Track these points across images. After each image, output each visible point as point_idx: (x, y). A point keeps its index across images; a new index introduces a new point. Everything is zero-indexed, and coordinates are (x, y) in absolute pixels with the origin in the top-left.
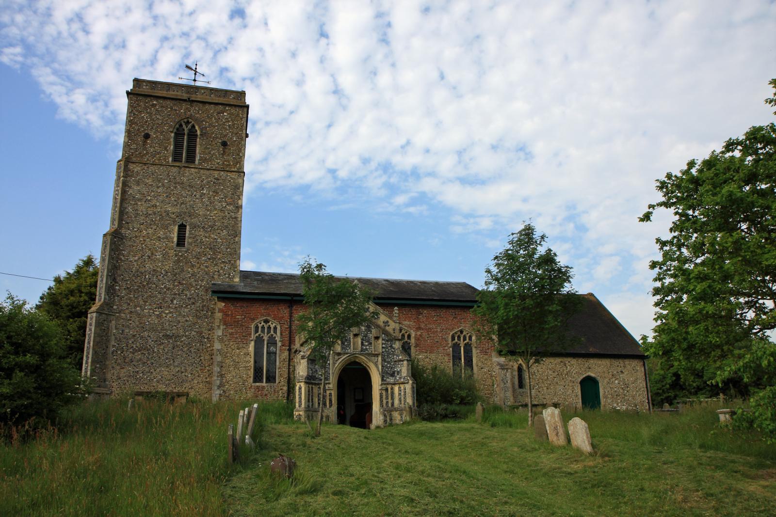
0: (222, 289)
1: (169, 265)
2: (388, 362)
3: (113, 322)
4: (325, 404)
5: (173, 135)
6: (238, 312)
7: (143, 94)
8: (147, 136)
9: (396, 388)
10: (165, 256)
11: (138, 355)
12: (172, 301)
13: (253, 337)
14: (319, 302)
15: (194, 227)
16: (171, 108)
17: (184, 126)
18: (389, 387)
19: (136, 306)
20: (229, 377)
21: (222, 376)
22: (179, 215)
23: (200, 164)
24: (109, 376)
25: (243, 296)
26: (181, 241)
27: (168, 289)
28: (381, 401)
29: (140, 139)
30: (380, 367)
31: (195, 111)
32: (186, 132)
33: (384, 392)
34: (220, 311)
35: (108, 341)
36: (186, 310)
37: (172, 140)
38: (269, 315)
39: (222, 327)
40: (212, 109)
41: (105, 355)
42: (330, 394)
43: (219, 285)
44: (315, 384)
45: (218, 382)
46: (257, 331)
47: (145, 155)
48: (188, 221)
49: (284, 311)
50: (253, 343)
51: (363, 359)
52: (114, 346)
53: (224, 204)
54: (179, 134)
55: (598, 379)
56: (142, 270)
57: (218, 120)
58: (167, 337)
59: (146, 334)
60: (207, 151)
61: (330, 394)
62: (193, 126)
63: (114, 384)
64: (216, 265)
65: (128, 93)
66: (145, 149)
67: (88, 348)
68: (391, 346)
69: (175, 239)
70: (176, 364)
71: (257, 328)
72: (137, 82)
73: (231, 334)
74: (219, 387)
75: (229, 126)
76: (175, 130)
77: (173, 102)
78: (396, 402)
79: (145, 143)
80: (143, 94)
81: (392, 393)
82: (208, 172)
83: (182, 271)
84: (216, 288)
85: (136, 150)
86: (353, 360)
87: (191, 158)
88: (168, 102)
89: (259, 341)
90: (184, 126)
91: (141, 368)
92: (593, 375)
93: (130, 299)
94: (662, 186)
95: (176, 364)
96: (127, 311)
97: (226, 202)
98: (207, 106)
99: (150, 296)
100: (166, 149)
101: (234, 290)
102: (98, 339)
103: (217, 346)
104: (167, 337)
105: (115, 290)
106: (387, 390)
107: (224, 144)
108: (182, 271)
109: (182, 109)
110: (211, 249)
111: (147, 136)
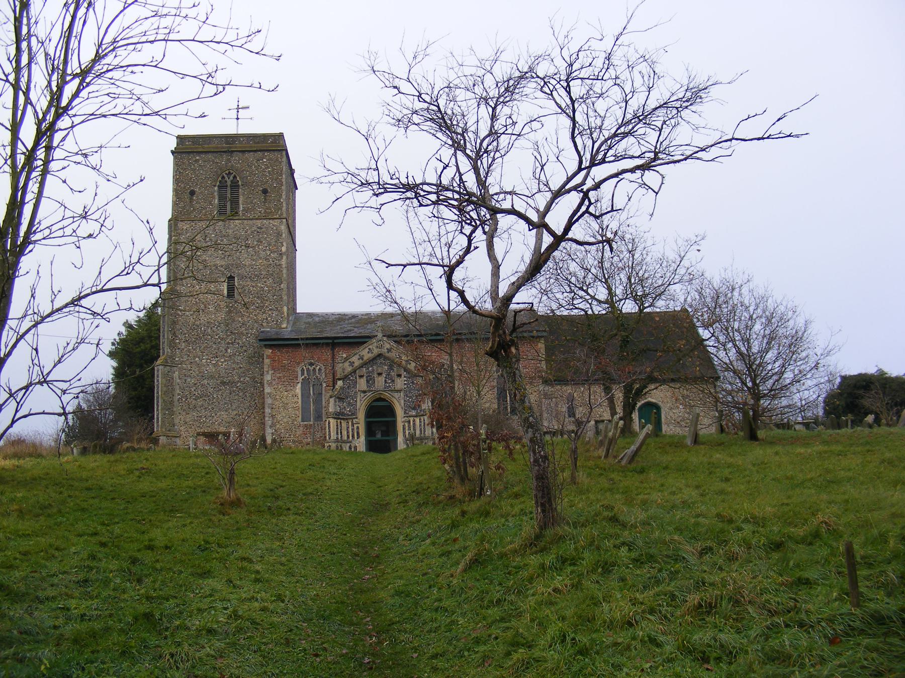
0: (269, 336)
1: (221, 316)
2: (410, 397)
3: (177, 373)
4: (353, 436)
5: (216, 188)
6: (285, 357)
7: (189, 150)
8: (192, 193)
9: (417, 420)
10: (218, 308)
11: (200, 402)
12: (226, 350)
13: (300, 379)
14: (337, 338)
15: (242, 277)
16: (213, 162)
17: (227, 178)
18: (411, 419)
19: (195, 357)
20: (279, 417)
21: (273, 416)
22: (227, 267)
23: (243, 214)
24: (177, 421)
25: (321, 341)
26: (231, 294)
27: (222, 339)
28: (404, 433)
29: (187, 196)
30: (402, 402)
31: (236, 161)
32: (229, 183)
33: (406, 424)
34: (268, 357)
35: (173, 390)
36: (239, 358)
37: (216, 194)
38: (313, 358)
39: (270, 372)
40: (250, 157)
41: (172, 402)
42: (358, 428)
43: (268, 332)
44: (344, 419)
45: (270, 422)
46: (303, 374)
47: (192, 212)
48: (236, 272)
49: (327, 353)
50: (299, 385)
51: (387, 395)
52: (179, 394)
53: (268, 253)
54: (222, 186)
55: (660, 404)
56: (198, 323)
57: (257, 168)
58: (223, 383)
59: (206, 381)
60: (249, 201)
61: (358, 428)
62: (235, 177)
63: (182, 428)
64: (264, 313)
65: (173, 152)
66: (191, 206)
67: (158, 398)
68: (413, 383)
69: (225, 292)
70: (234, 407)
71: (303, 370)
72: (181, 139)
73: (279, 378)
74: (271, 427)
75: (269, 172)
76: (218, 183)
77: (215, 154)
78: (418, 432)
79: (191, 200)
80: (189, 150)
81: (414, 424)
82: (250, 222)
83: (234, 321)
84: (262, 336)
85: (184, 208)
86: (378, 397)
87: (235, 213)
88: (210, 156)
89: (305, 382)
90: (227, 178)
91: (203, 413)
92: (654, 401)
93: (189, 350)
94: (124, 324)
95: (234, 407)
96: (187, 362)
97: (270, 250)
98: (247, 155)
99: (206, 347)
100: (211, 204)
101: (279, 337)
102: (165, 389)
103: (267, 390)
104: (223, 383)
105: (175, 343)
106: (409, 422)
107: (265, 192)
108: (234, 321)
109: (223, 161)
110: (258, 298)
111: (192, 193)
